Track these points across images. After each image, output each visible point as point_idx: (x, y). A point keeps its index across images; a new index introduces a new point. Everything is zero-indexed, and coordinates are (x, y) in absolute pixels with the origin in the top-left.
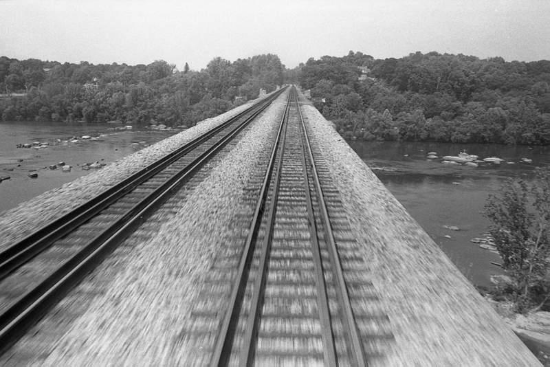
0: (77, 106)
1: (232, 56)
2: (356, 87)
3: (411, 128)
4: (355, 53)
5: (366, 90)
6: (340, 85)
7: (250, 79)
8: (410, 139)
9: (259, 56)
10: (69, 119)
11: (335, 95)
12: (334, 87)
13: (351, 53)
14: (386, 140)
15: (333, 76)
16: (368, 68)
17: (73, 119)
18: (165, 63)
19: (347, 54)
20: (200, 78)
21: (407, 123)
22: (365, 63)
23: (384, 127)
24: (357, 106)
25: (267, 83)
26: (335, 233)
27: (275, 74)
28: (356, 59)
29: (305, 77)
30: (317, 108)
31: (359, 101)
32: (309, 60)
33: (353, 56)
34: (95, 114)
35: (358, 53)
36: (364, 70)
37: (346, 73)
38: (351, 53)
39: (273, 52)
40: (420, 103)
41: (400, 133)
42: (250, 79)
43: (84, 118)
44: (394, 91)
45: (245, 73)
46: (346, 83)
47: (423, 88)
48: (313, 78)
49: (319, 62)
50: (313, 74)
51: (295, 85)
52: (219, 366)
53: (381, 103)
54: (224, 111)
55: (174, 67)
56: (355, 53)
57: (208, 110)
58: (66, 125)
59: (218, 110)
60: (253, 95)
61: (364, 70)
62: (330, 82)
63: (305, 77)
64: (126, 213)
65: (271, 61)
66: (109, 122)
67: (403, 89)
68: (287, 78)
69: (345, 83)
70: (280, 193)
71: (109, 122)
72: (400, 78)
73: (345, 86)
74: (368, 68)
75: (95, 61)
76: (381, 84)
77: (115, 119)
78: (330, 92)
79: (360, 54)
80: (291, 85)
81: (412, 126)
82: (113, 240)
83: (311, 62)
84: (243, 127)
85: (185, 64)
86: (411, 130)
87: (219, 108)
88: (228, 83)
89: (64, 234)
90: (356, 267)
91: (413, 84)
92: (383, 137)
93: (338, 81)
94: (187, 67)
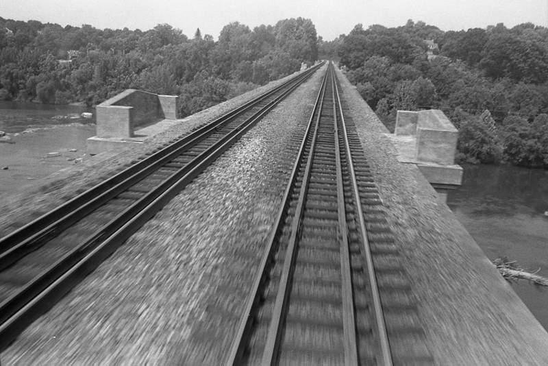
0: (32, 80)
1: (252, 23)
2: (425, 69)
3: (531, 146)
4: (415, 23)
5: (439, 74)
6: (393, 65)
7: (271, 51)
8: (525, 164)
9: (287, 19)
10: (20, 97)
11: (393, 81)
12: (392, 68)
13: (410, 22)
14: (482, 162)
15: (391, 52)
16: (435, 42)
17: (26, 98)
18: (170, 27)
19: (403, 23)
20: (203, 47)
21: (522, 136)
22: (431, 35)
23: (483, 142)
24: (427, 98)
25: (294, 57)
26: (384, 296)
27: (305, 44)
28: (420, 31)
29: (350, 51)
30: (365, 99)
31: (432, 92)
32: (359, 25)
33: (412, 27)
34: (51, 92)
35: (420, 22)
36: (432, 45)
37: (410, 46)
38: (410, 22)
39: (305, 16)
40: (531, 99)
41: (506, 151)
42: (271, 51)
43: (38, 96)
44: (480, 77)
45: (265, 42)
46: (409, 62)
47: (529, 74)
48: (360, 53)
49: (367, 33)
50: (360, 47)
51: (333, 63)
52: (233, 365)
53: (467, 96)
54: (222, 99)
55: (181, 32)
56: (415, 23)
57: (200, 94)
58: (14, 107)
59: (214, 96)
60: (271, 75)
61: (432, 45)
62: (385, 59)
63: (350, 51)
64: (173, 175)
65: (301, 28)
66: (71, 104)
67: (494, 74)
68: (324, 53)
69: (407, 63)
70: (313, 170)
71: (71, 104)
72: (493, 58)
73: (408, 67)
74: (435, 42)
75: (100, 25)
76: (459, 66)
77: (78, 101)
78: (385, 75)
79: (422, 25)
80: (328, 62)
81: (531, 142)
82: (154, 205)
83: (358, 30)
84: (265, 114)
85: (196, 31)
86: (531, 151)
87: (215, 93)
88: (240, 56)
89: (114, 196)
90: (369, 218)
91: (513, 67)
92: (478, 158)
93: (397, 58)
94: (198, 33)
